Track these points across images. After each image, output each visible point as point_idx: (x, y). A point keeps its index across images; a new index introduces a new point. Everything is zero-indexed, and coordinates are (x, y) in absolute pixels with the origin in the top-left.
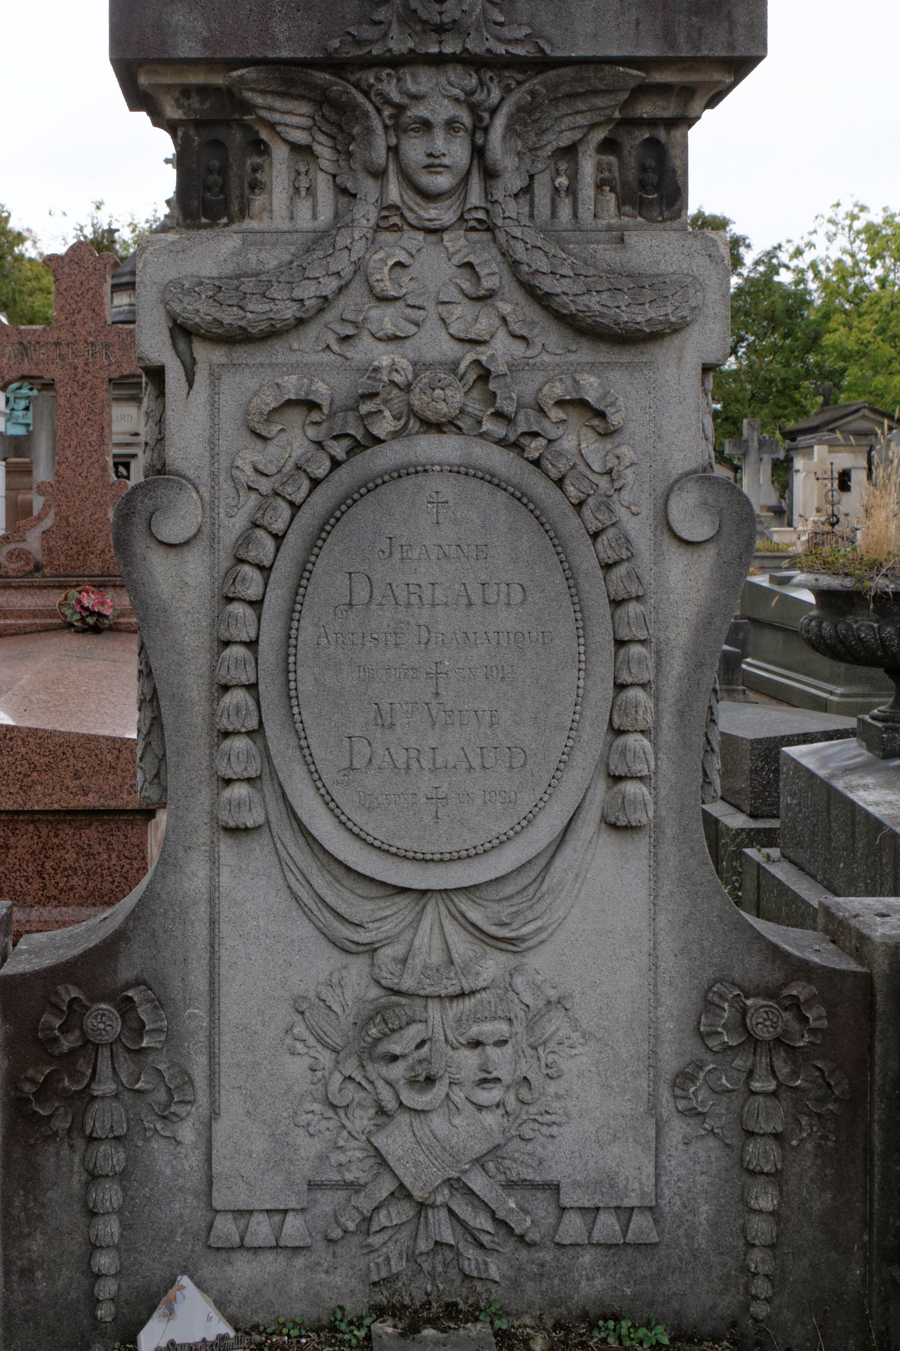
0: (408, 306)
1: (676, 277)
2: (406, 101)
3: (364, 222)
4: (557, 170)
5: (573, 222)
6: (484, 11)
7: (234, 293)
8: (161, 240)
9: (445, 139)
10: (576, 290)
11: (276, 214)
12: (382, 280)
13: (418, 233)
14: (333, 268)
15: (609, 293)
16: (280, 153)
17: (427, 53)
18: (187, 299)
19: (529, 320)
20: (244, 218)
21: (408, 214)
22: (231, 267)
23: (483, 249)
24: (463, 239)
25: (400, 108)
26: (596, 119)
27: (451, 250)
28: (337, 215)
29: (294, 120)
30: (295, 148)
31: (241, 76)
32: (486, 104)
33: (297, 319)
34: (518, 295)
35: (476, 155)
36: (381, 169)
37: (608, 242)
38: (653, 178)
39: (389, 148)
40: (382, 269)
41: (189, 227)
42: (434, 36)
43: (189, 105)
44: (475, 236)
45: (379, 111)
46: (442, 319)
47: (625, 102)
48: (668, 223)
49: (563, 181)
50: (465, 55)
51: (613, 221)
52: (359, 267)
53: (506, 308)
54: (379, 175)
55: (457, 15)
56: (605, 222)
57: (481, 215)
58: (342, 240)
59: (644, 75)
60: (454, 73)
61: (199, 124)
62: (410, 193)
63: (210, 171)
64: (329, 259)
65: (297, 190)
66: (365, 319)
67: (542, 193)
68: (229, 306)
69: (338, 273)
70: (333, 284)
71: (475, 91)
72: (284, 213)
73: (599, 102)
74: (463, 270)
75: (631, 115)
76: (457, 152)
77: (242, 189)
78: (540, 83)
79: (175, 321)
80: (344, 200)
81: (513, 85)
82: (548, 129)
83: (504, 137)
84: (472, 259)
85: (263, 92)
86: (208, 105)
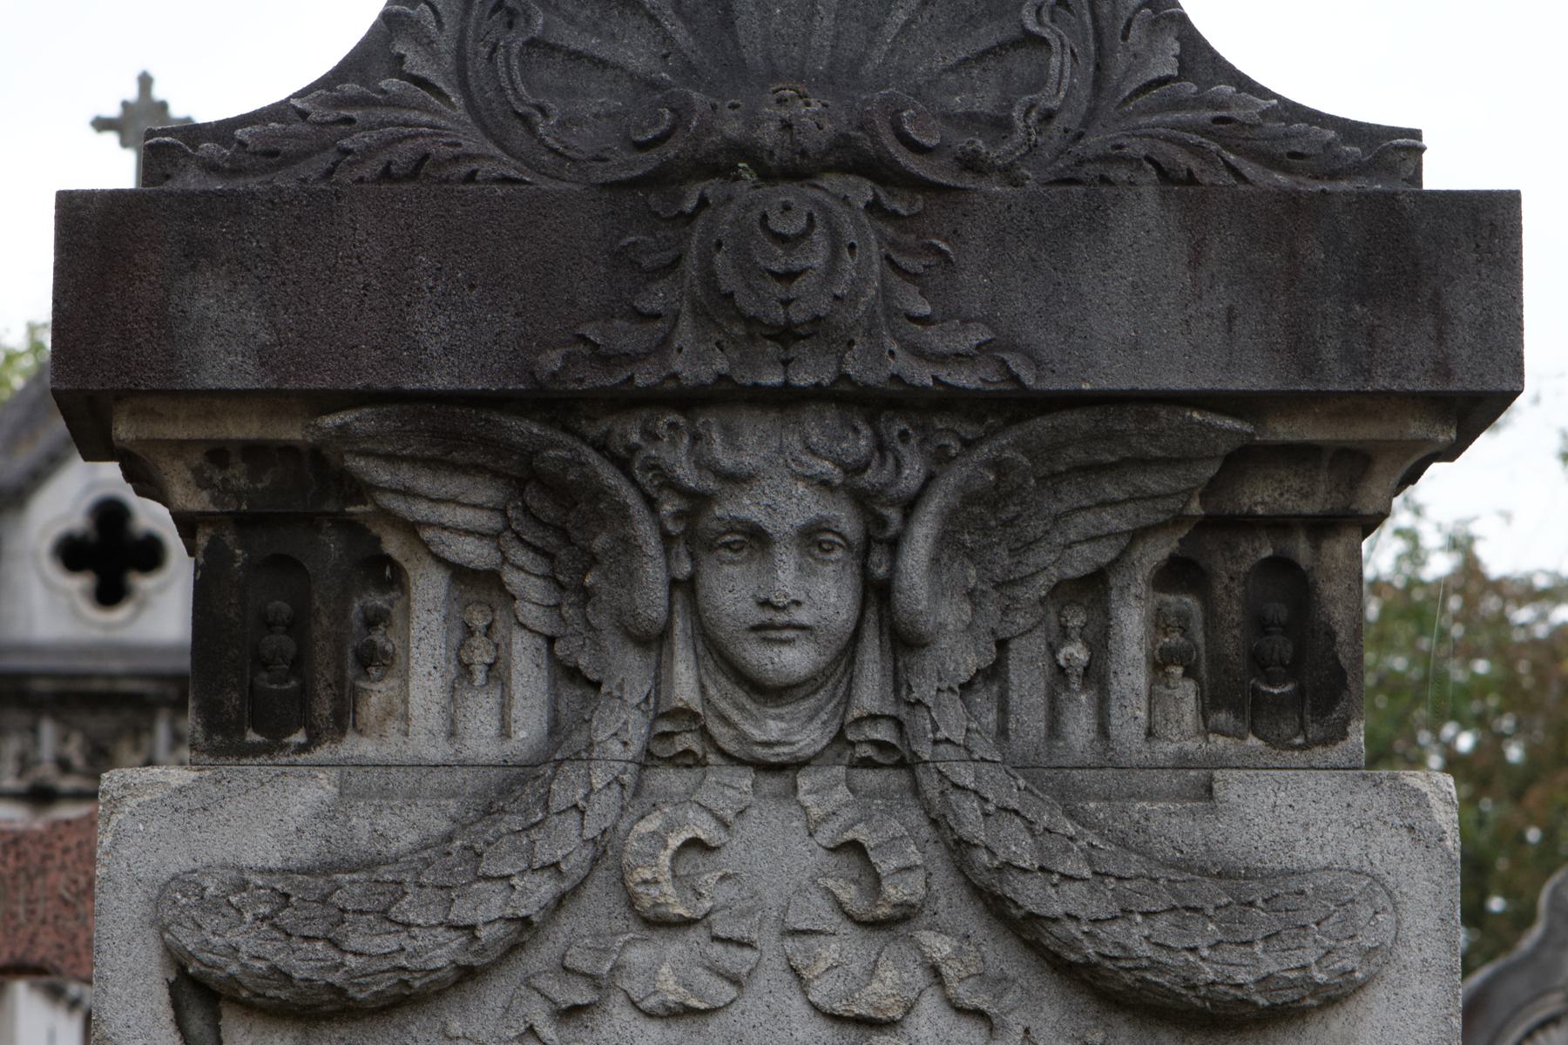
0: (716, 939)
1: (1328, 878)
2: (711, 484)
3: (616, 748)
4: (1063, 628)
5: (1098, 746)
6: (885, 292)
7: (317, 910)
8: (154, 784)
9: (800, 568)
10: (1097, 908)
11: (417, 725)
12: (656, 882)
13: (740, 771)
14: (544, 855)
15: (1171, 917)
16: (428, 589)
17: (756, 385)
18: (211, 922)
19: (993, 972)
20: (343, 733)
21: (717, 729)
22: (312, 847)
23: (889, 811)
24: (842, 788)
25: (699, 501)
26: (1147, 517)
27: (816, 812)
28: (555, 728)
29: (462, 516)
30: (460, 574)
31: (343, 428)
32: (893, 491)
33: (459, 967)
34: (969, 918)
35: (872, 597)
36: (655, 631)
37: (1179, 796)
38: (1281, 646)
39: (674, 583)
40: (655, 856)
41: (216, 752)
42: (771, 348)
43: (225, 481)
44: (871, 778)
45: (651, 503)
46: (794, 970)
47: (1212, 480)
48: (1319, 750)
49: (1076, 652)
50: (844, 387)
51: (1190, 746)
52: (603, 850)
53: (940, 946)
54: (654, 641)
55: (824, 306)
56: (1172, 748)
57: (883, 733)
58: (565, 791)
59: (1248, 428)
60: (817, 427)
61: (245, 523)
62: (723, 680)
63: (268, 625)
64: (534, 834)
65: (466, 669)
66: (616, 968)
67: (1027, 682)
68: (307, 938)
69: (556, 865)
70: (545, 889)
71: (868, 465)
72: (436, 721)
73: (1152, 482)
74: (842, 859)
75: (1228, 508)
76: (829, 596)
77: (341, 668)
78: (1014, 446)
79: (182, 969)
80: (572, 695)
81: (955, 447)
82: (1037, 540)
83: (935, 560)
84: (861, 833)
85: (391, 458)
86: (265, 482)
